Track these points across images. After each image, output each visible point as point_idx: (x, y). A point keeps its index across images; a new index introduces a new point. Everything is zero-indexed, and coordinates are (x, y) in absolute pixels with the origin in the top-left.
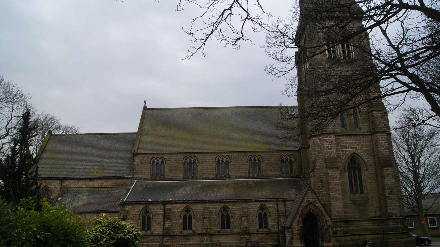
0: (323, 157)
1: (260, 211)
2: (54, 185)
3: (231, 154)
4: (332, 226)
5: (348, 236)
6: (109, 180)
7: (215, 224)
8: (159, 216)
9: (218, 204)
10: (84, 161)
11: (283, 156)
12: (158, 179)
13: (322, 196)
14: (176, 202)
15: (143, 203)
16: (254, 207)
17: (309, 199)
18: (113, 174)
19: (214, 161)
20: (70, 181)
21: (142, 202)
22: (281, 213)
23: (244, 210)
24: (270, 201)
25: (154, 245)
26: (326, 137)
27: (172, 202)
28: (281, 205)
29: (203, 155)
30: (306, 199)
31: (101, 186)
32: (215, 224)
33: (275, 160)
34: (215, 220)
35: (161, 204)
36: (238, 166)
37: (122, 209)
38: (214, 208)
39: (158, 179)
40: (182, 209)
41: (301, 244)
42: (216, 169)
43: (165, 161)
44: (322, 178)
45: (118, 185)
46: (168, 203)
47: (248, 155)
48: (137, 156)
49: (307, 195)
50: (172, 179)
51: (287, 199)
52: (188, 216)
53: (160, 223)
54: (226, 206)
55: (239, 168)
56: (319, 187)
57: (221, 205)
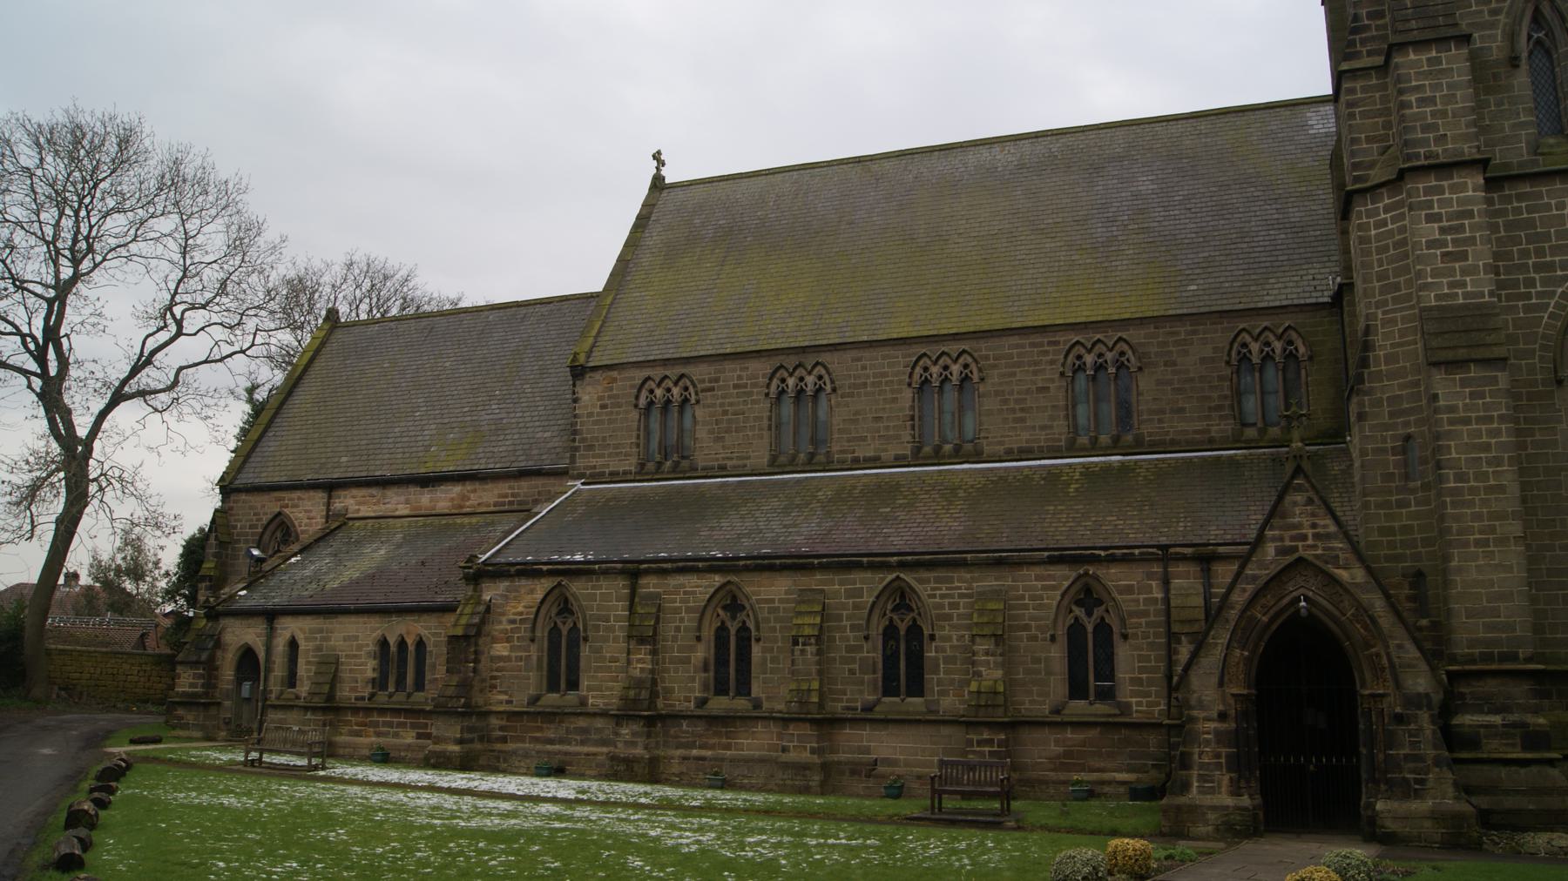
0: (1412, 307)
1: (1074, 608)
2: (306, 511)
3: (983, 345)
4: (1437, 698)
5: (1551, 762)
6: (487, 484)
7: (852, 672)
8: (611, 629)
9: (869, 575)
10: (418, 414)
11: (1248, 339)
12: (668, 472)
13: (1406, 529)
14: (681, 564)
15: (548, 570)
16: (1045, 588)
17: (1293, 538)
18: (503, 460)
19: (907, 380)
20: (355, 492)
21: (545, 568)
22: (1182, 622)
23: (991, 606)
24: (1126, 559)
25: (587, 754)
26: (1428, 191)
27: (665, 566)
28: (1186, 582)
29: (854, 353)
30: (1274, 539)
31: (461, 507)
32: (852, 672)
33: (1203, 360)
34: (850, 649)
35: (622, 572)
36: (1016, 396)
37: (471, 597)
38: (849, 594)
39: (668, 472)
40: (708, 596)
41: (1236, 792)
42: (912, 418)
43: (697, 394)
44: (1407, 424)
45: (520, 503)
46: (647, 572)
47: (1065, 342)
48: (588, 376)
49: (1284, 516)
50: (723, 471)
51: (1221, 549)
52: (733, 632)
53: (614, 660)
54: (903, 584)
55: (1022, 410)
56: (1389, 477)
57: (883, 579)
